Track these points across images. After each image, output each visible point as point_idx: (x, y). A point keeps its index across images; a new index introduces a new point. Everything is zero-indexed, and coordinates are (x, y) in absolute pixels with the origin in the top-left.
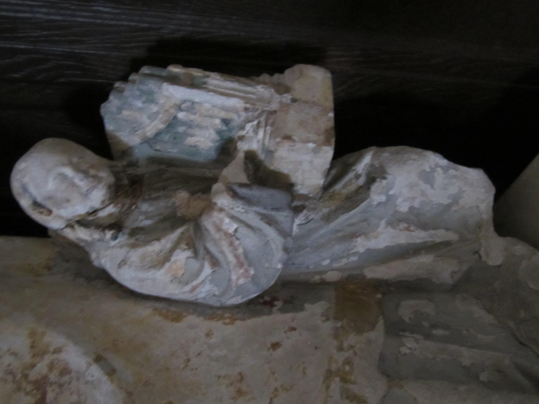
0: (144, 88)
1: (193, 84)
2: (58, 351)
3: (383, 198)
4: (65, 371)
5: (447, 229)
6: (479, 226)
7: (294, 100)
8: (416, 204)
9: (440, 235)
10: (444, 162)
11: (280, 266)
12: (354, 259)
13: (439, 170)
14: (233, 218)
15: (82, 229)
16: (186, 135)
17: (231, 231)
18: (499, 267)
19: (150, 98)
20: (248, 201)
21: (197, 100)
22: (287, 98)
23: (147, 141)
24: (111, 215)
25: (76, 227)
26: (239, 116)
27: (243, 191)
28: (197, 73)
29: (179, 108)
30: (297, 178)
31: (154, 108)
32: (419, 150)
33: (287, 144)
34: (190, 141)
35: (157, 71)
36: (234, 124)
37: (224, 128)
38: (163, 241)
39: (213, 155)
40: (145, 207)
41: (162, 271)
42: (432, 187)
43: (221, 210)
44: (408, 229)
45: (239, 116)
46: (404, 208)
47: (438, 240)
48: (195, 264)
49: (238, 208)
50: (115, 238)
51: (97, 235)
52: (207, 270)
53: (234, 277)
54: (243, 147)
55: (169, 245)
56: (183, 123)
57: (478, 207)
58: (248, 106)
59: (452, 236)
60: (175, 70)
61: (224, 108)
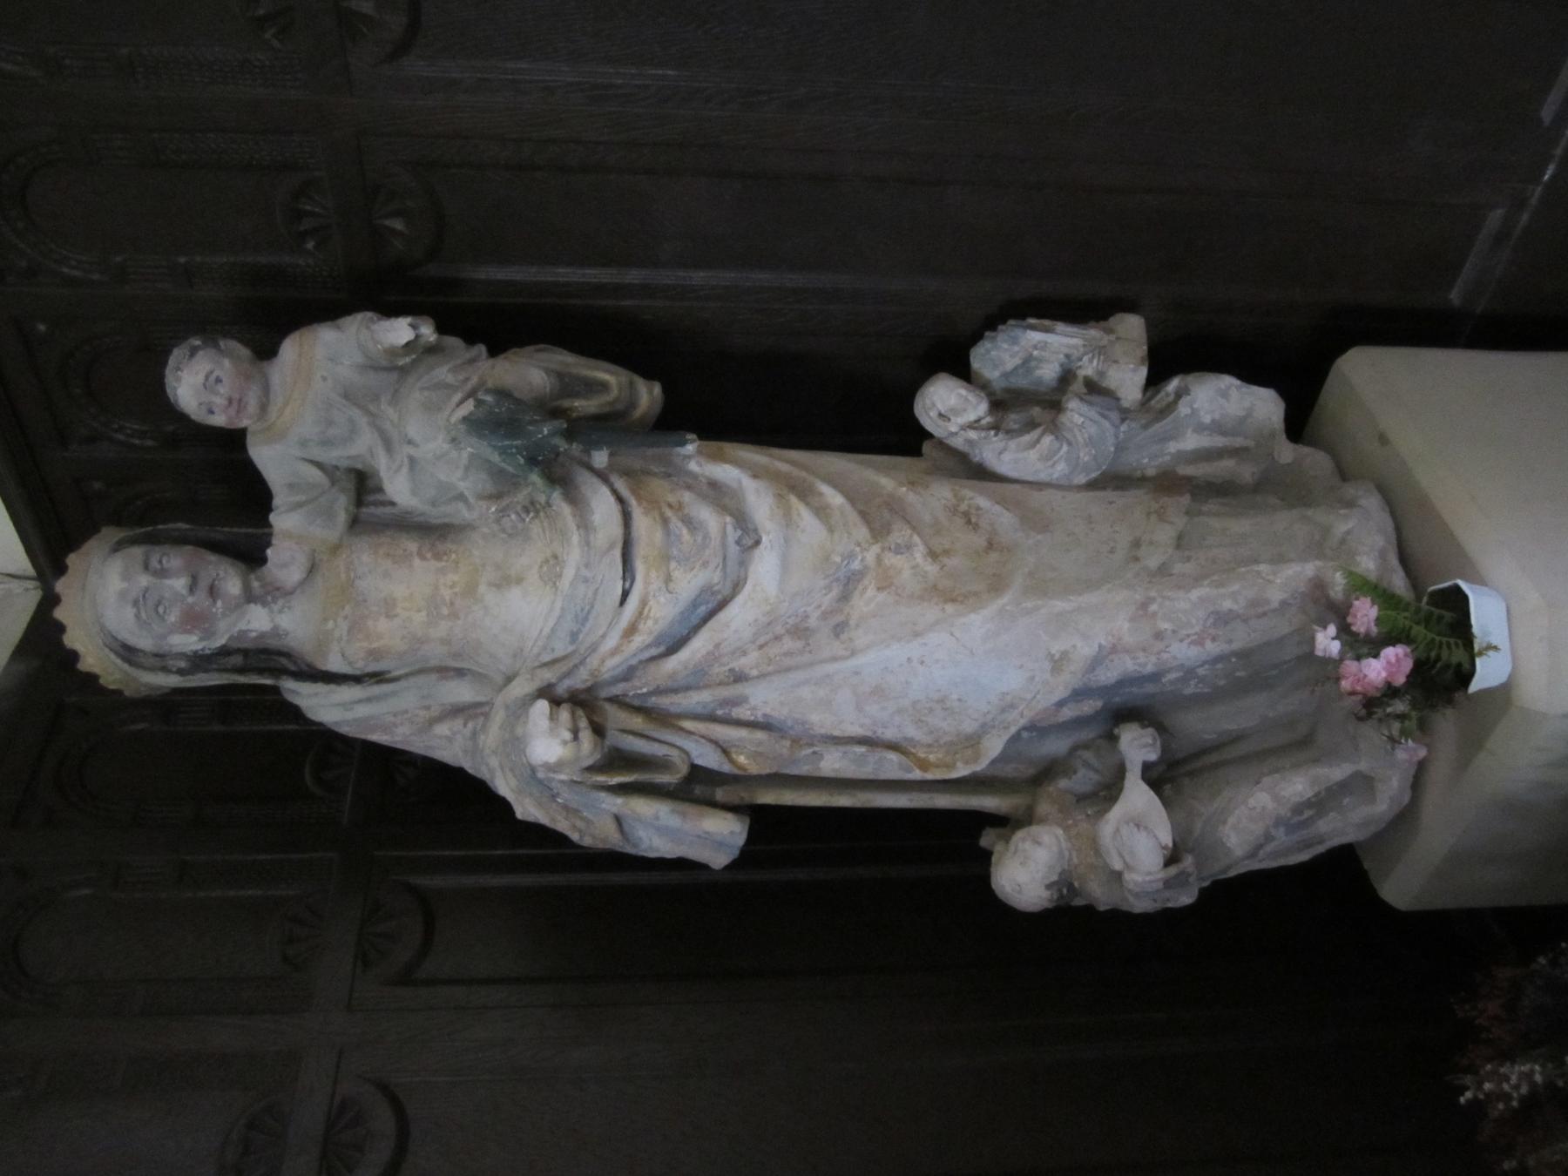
0: (1013, 334)
1: (1047, 330)
2: (971, 499)
3: (1188, 411)
4: (978, 508)
5: (1246, 438)
6: (1273, 435)
7: (1118, 338)
8: (1217, 416)
9: (1239, 442)
10: (1237, 382)
11: (1112, 449)
12: (1168, 458)
13: (1233, 388)
14: (1081, 415)
15: (972, 431)
16: (1037, 368)
17: (1080, 423)
18: (1288, 464)
19: (1015, 341)
20: (1090, 404)
21: (1049, 341)
22: (1112, 337)
23: (1006, 375)
24: (988, 423)
25: (968, 429)
26: (1078, 351)
27: (1084, 397)
28: (1047, 322)
29: (1035, 347)
30: (1121, 394)
31: (1016, 348)
32: (1217, 375)
33: (1115, 366)
34: (1039, 373)
35: (1020, 322)
36: (1073, 358)
37: (1067, 361)
38: (1032, 434)
39: (1054, 384)
40: (1013, 416)
41: (1035, 450)
42: (1228, 401)
43: (1072, 410)
44: (1211, 435)
45: (1078, 351)
46: (1207, 419)
47: (1237, 445)
48: (1057, 445)
49: (1085, 408)
50: (996, 435)
51: (983, 434)
52: (1065, 448)
53: (1082, 455)
54: (1082, 373)
55: (1036, 437)
56: (1036, 359)
57: (1270, 419)
58: (1086, 343)
59: (1250, 443)
60: (1032, 321)
61: (1068, 346)
